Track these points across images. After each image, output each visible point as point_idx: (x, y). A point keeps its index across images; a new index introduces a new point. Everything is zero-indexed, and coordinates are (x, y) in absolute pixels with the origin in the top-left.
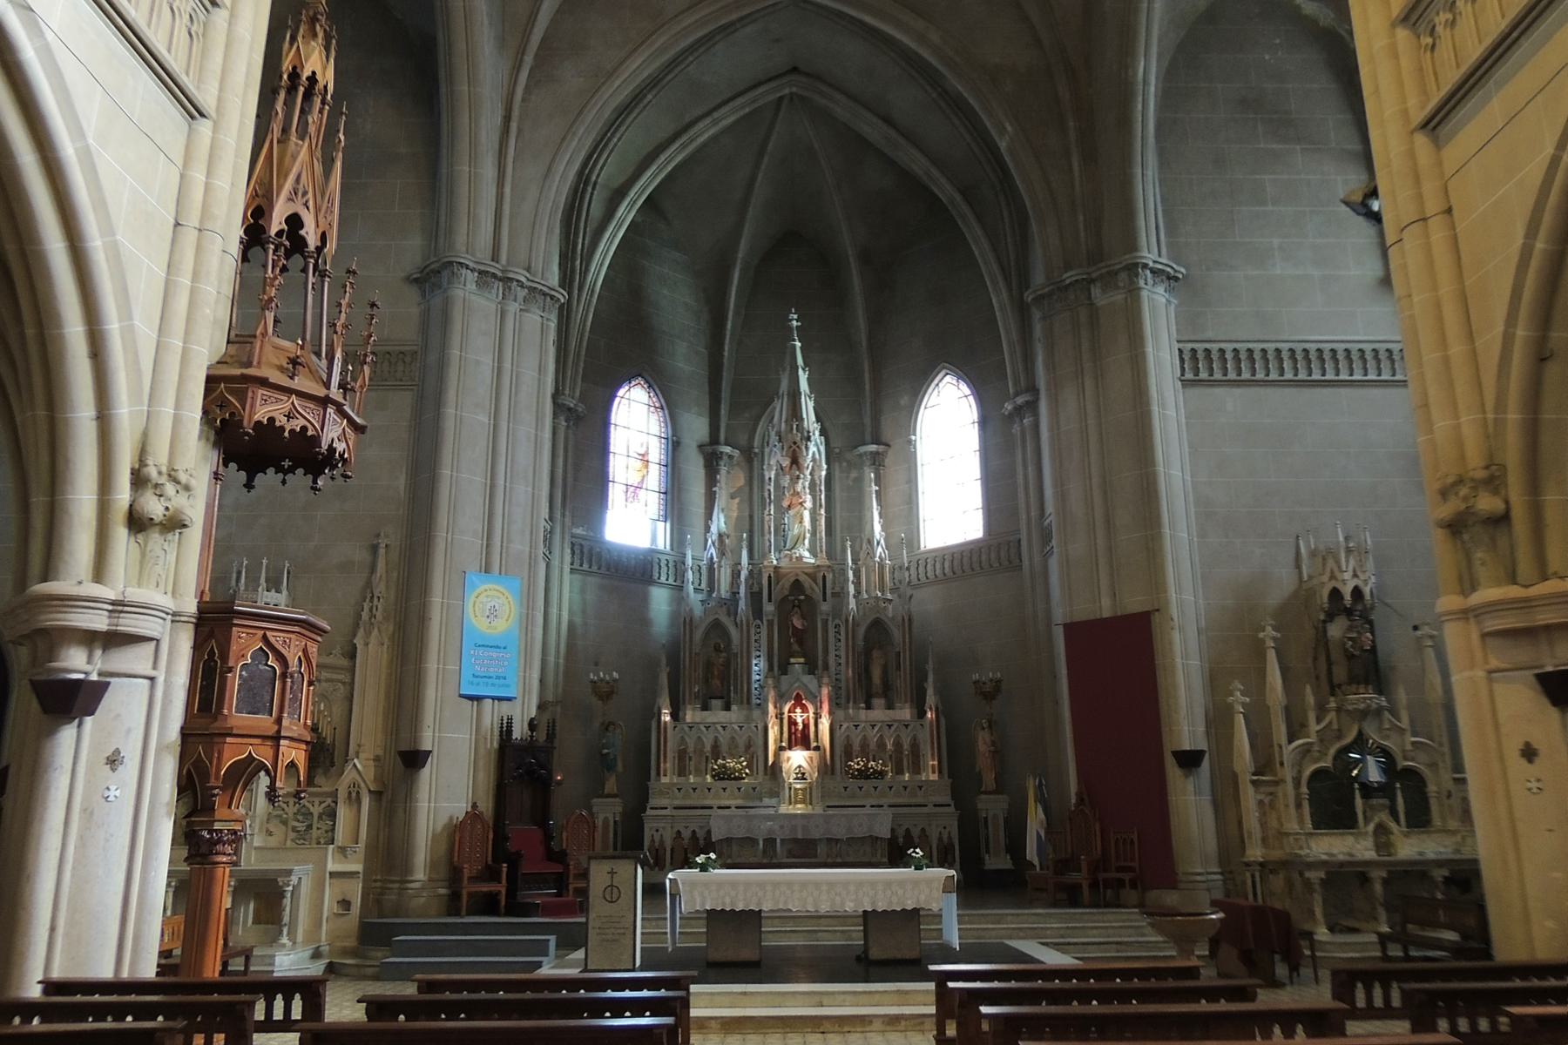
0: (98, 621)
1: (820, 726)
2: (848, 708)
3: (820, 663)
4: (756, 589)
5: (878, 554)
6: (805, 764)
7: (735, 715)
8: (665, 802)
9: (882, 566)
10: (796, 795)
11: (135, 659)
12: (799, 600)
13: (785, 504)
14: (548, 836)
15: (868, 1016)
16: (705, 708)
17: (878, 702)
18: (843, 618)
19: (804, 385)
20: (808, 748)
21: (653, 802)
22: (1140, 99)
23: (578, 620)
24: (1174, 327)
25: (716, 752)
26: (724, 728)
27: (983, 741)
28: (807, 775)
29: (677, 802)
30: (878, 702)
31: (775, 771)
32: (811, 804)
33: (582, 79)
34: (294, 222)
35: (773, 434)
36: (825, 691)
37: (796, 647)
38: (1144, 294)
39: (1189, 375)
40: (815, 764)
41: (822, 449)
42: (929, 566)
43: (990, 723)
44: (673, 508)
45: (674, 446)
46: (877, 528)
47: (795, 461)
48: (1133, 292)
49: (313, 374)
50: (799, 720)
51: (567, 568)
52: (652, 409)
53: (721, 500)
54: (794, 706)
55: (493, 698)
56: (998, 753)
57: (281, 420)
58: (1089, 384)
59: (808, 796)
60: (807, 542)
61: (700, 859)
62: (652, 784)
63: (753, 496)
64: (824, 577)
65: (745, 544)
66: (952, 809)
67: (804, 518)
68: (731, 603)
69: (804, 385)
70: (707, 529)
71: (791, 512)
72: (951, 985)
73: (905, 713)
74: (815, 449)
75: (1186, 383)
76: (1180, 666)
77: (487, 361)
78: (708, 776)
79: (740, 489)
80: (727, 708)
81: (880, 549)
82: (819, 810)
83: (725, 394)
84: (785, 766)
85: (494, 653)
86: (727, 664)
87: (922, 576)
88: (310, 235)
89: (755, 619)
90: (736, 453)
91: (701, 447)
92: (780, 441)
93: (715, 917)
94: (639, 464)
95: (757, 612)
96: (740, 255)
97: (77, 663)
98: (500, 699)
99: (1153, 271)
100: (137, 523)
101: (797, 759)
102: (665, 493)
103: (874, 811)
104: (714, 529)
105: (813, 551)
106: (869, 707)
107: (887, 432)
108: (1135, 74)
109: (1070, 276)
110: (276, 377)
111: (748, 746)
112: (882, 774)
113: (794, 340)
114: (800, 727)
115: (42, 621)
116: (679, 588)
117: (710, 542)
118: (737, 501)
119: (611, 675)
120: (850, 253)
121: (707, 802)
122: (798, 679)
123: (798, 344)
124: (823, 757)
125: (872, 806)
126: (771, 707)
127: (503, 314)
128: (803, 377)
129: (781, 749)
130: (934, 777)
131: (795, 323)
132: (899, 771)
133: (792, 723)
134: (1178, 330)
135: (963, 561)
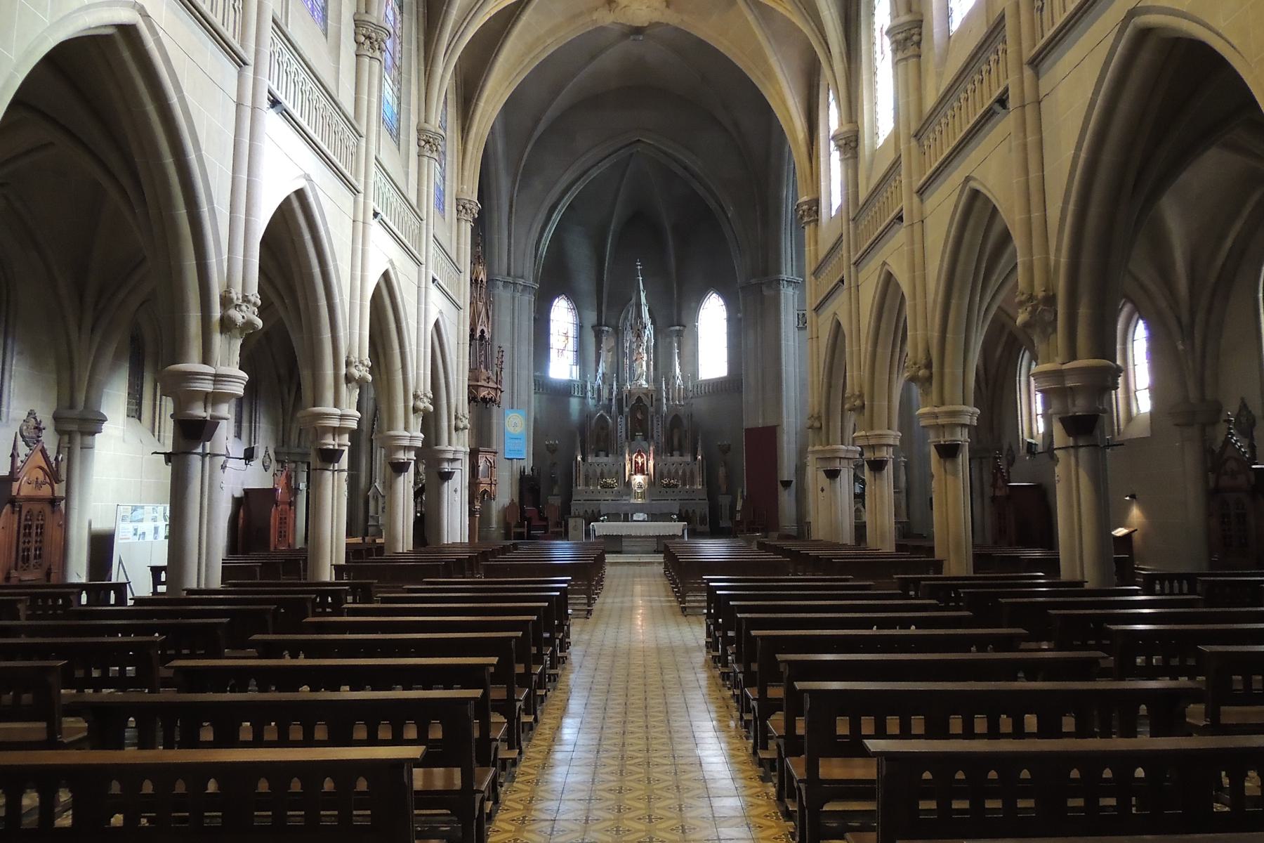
0: (208, 387)
1: (649, 464)
2: (662, 456)
3: (650, 434)
4: (620, 397)
6: (642, 482)
9: (679, 389)
11: (457, 465)
12: (641, 406)
13: (634, 358)
14: (540, 512)
19: (643, 300)
20: (644, 474)
21: (574, 498)
22: (784, 206)
23: (538, 416)
24: (796, 303)
25: (602, 476)
26: (606, 465)
27: (722, 471)
29: (585, 498)
31: (629, 484)
34: (482, 331)
35: (628, 324)
36: (651, 448)
37: (638, 428)
38: (782, 292)
39: (801, 326)
40: (647, 481)
41: (652, 332)
44: (580, 359)
45: (580, 327)
46: (678, 370)
47: (639, 336)
48: (778, 291)
49: (493, 381)
50: (640, 462)
51: (533, 392)
52: (570, 310)
53: (603, 353)
55: (517, 459)
57: (487, 396)
58: (759, 329)
59: (643, 495)
60: (644, 377)
61: (602, 519)
62: (574, 489)
63: (618, 351)
64: (652, 395)
65: (615, 379)
66: (707, 501)
67: (643, 365)
68: (608, 408)
69: (643, 300)
70: (597, 371)
71: (637, 362)
72: (711, 584)
73: (688, 458)
74: (648, 332)
75: (799, 329)
76: (785, 449)
77: (508, 319)
78: (599, 487)
79: (612, 347)
80: (607, 456)
82: (648, 501)
84: (633, 482)
85: (517, 441)
86: (607, 435)
87: (699, 392)
88: (487, 335)
90: (610, 329)
92: (632, 329)
94: (564, 338)
95: (621, 411)
96: (612, 228)
97: (446, 467)
98: (519, 459)
99: (786, 281)
100: (457, 429)
101: (639, 479)
102: (576, 351)
103: (673, 502)
104: (600, 371)
105: (647, 381)
106: (672, 455)
107: (684, 321)
108: (782, 194)
109: (753, 281)
110: (486, 384)
111: (617, 473)
112: (676, 486)
113: (639, 276)
114: (640, 464)
115: (183, 387)
116: (584, 397)
117: (598, 377)
118: (611, 353)
119: (555, 442)
121: (599, 498)
123: (641, 278)
124: (650, 479)
126: (627, 456)
127: (513, 298)
129: (631, 475)
130: (700, 487)
132: (684, 484)
133: (637, 463)
134: (798, 305)
135: (717, 386)
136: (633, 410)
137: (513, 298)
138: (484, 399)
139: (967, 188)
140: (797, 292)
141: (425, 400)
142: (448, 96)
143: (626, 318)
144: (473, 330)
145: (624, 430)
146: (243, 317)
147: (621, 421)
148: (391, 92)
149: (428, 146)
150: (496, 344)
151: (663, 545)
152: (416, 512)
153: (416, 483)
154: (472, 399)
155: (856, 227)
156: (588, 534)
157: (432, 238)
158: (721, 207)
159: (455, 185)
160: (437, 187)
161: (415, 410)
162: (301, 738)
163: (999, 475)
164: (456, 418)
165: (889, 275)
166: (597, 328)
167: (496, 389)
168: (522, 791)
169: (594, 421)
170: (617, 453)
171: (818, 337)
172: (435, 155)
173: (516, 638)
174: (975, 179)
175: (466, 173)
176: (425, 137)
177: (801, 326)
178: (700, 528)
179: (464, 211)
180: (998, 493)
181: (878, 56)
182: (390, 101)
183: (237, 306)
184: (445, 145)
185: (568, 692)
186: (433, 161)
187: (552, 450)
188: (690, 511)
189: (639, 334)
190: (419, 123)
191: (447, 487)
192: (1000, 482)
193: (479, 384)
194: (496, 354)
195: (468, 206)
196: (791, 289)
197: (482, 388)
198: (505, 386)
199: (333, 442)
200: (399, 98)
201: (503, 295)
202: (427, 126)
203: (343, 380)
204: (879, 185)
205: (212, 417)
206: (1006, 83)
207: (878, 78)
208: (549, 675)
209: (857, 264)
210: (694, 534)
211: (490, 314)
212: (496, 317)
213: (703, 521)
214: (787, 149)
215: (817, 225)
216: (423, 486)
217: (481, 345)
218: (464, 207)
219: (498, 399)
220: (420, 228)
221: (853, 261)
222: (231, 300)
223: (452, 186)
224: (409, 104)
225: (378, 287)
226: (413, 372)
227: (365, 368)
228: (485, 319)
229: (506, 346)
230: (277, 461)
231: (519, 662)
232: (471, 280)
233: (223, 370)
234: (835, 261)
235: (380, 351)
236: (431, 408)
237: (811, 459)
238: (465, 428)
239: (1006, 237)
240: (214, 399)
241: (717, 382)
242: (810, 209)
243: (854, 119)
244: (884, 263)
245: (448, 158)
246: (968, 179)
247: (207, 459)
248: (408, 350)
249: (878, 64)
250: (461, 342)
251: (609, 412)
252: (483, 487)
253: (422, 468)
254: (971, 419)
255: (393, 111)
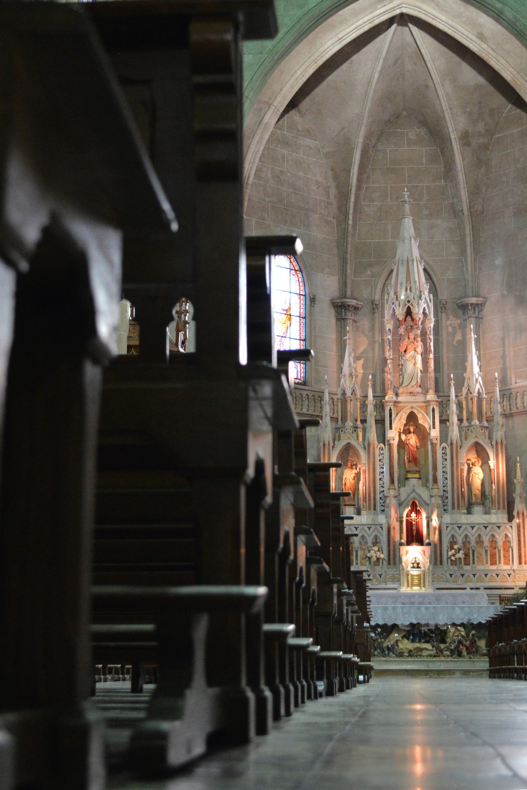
5: (477, 390)
10: (412, 579)
15: (454, 670)
17: (478, 509)
18: (449, 441)
28: (421, 565)
30: (478, 509)
32: (424, 586)
33: (251, 56)
41: (431, 305)
42: (518, 397)
54: (411, 512)
59: (421, 581)
74: (425, 305)
81: (478, 386)
89: (379, 443)
102: (304, 340)
103: (473, 591)
106: (469, 512)
120: (452, 137)
122: (414, 491)
125: (472, 589)
145: (386, 469)
170: (375, 509)
189: (409, 308)
204: (522, 387)
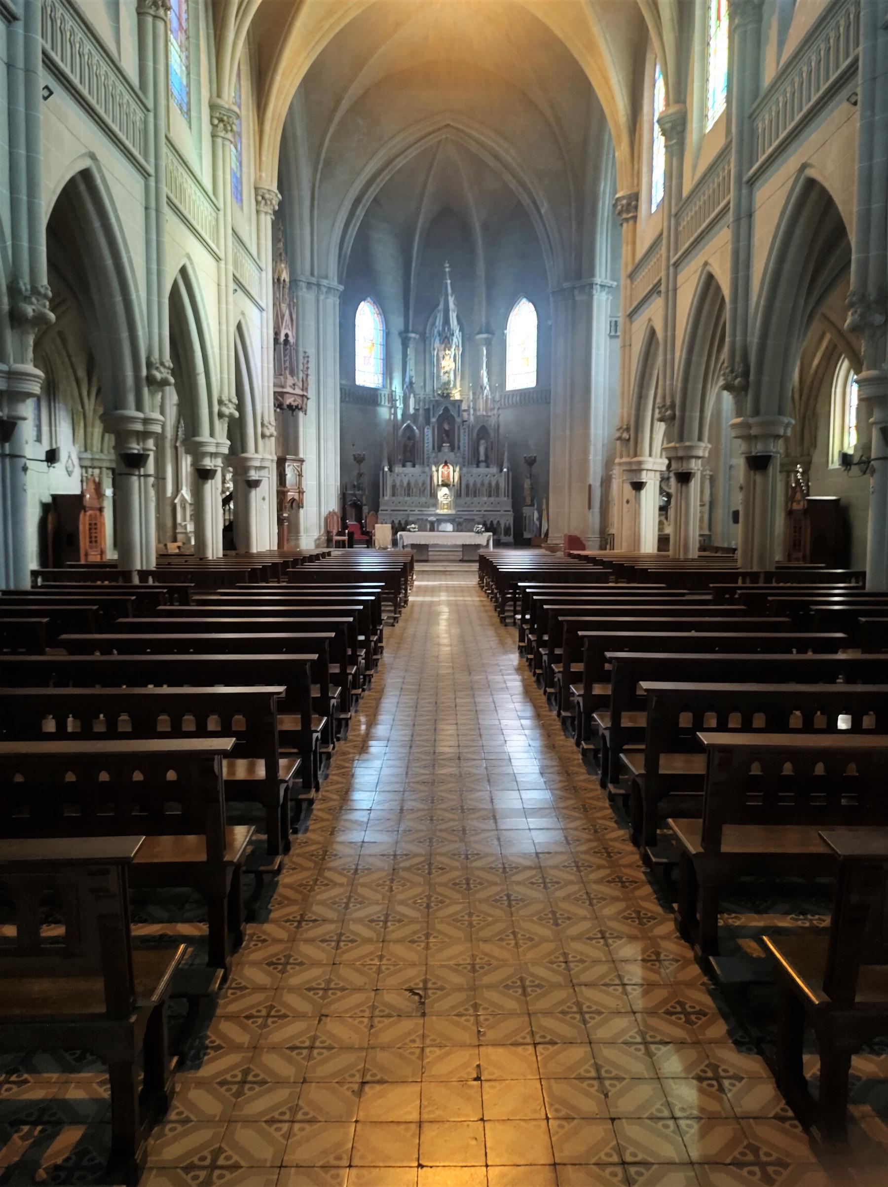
0: (139, 427)
7: (418, 469)
8: (386, 508)
11: (265, 473)
16: (404, 466)
17: (483, 464)
21: (381, 508)
27: (527, 484)
30: (483, 464)
34: (287, 335)
37: (445, 438)
38: (595, 297)
39: (613, 333)
43: (531, 475)
45: (387, 335)
48: (591, 296)
56: (532, 488)
57: (293, 404)
62: (381, 500)
66: (511, 513)
68: (415, 417)
69: (451, 305)
73: (494, 470)
75: (611, 337)
80: (414, 466)
83: (412, 305)
86: (414, 445)
88: (291, 339)
90: (417, 336)
91: (400, 334)
93: (413, 546)
95: (428, 422)
97: (254, 475)
100: (263, 436)
110: (290, 390)
127: (318, 301)
128: (451, 300)
131: (447, 270)
135: (524, 395)
136: (442, 419)
137: (318, 301)
138: (290, 407)
139: (803, 177)
140: (611, 298)
141: (230, 405)
142: (242, 67)
143: (434, 324)
144: (277, 334)
145: (431, 439)
146: (34, 310)
147: (428, 432)
148: (178, 60)
149: (221, 125)
150: (301, 349)
151: (468, 553)
152: (225, 520)
153: (223, 492)
154: (279, 405)
155: (677, 224)
156: (395, 543)
157: (230, 231)
158: (535, 202)
159: (252, 171)
160: (233, 174)
161: (221, 415)
162: (129, 729)
163: (798, 489)
164: (263, 425)
165: (710, 277)
166: (404, 335)
167: (303, 396)
168: (338, 783)
169: (401, 431)
171: (630, 345)
172: (229, 136)
173: (312, 661)
174: (811, 166)
175: (264, 158)
176: (218, 115)
177: (613, 333)
178: (504, 539)
179: (263, 202)
180: (795, 507)
181: (713, 22)
182: (178, 71)
183: (157, 368)
184: (240, 125)
185: (381, 692)
186: (227, 143)
187: (359, 460)
188: (495, 522)
190: (211, 97)
191: (255, 496)
192: (798, 496)
193: (285, 390)
194: (301, 360)
195: (267, 196)
196: (604, 294)
197: (287, 395)
198: (311, 393)
199: (138, 447)
200: (187, 68)
201: (307, 296)
202: (220, 102)
203: (144, 382)
205: (8, 417)
206: (856, 52)
207: (712, 49)
208: (321, 753)
209: (676, 265)
210: (498, 544)
211: (294, 316)
212: (301, 322)
213: (507, 532)
214: (606, 137)
215: (635, 222)
216: (231, 494)
217: (285, 350)
218: (263, 198)
219: (304, 406)
220: (217, 220)
221: (673, 261)
222: (19, 291)
223: (249, 173)
224: (199, 75)
225: (175, 285)
226: (216, 376)
227: (166, 370)
228: (289, 322)
229: (312, 352)
230: (82, 467)
231: (333, 661)
232: (273, 279)
233: (220, 441)
234: (652, 262)
235: (181, 352)
236: (237, 414)
237: (616, 471)
238: (271, 436)
239: (840, 231)
240: (144, 435)
241: (525, 393)
242: (629, 204)
243: (682, 98)
244: (706, 264)
245: (244, 140)
246: (804, 166)
247: (142, 478)
248: (134, 297)
249: (712, 31)
250: (265, 346)
251: (415, 422)
252: (290, 495)
253: (229, 476)
254: (785, 430)
255: (181, 83)
